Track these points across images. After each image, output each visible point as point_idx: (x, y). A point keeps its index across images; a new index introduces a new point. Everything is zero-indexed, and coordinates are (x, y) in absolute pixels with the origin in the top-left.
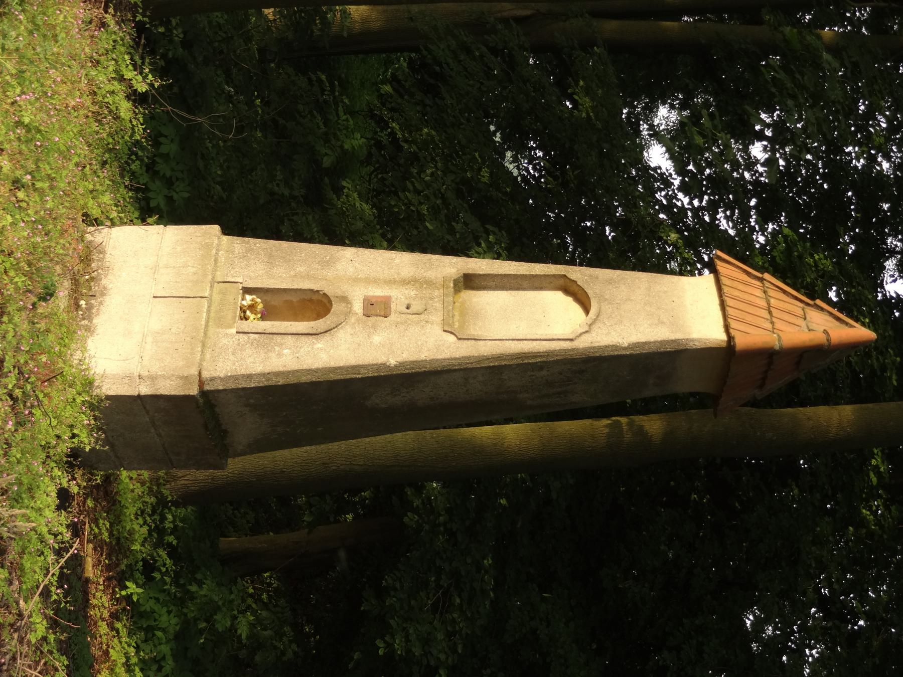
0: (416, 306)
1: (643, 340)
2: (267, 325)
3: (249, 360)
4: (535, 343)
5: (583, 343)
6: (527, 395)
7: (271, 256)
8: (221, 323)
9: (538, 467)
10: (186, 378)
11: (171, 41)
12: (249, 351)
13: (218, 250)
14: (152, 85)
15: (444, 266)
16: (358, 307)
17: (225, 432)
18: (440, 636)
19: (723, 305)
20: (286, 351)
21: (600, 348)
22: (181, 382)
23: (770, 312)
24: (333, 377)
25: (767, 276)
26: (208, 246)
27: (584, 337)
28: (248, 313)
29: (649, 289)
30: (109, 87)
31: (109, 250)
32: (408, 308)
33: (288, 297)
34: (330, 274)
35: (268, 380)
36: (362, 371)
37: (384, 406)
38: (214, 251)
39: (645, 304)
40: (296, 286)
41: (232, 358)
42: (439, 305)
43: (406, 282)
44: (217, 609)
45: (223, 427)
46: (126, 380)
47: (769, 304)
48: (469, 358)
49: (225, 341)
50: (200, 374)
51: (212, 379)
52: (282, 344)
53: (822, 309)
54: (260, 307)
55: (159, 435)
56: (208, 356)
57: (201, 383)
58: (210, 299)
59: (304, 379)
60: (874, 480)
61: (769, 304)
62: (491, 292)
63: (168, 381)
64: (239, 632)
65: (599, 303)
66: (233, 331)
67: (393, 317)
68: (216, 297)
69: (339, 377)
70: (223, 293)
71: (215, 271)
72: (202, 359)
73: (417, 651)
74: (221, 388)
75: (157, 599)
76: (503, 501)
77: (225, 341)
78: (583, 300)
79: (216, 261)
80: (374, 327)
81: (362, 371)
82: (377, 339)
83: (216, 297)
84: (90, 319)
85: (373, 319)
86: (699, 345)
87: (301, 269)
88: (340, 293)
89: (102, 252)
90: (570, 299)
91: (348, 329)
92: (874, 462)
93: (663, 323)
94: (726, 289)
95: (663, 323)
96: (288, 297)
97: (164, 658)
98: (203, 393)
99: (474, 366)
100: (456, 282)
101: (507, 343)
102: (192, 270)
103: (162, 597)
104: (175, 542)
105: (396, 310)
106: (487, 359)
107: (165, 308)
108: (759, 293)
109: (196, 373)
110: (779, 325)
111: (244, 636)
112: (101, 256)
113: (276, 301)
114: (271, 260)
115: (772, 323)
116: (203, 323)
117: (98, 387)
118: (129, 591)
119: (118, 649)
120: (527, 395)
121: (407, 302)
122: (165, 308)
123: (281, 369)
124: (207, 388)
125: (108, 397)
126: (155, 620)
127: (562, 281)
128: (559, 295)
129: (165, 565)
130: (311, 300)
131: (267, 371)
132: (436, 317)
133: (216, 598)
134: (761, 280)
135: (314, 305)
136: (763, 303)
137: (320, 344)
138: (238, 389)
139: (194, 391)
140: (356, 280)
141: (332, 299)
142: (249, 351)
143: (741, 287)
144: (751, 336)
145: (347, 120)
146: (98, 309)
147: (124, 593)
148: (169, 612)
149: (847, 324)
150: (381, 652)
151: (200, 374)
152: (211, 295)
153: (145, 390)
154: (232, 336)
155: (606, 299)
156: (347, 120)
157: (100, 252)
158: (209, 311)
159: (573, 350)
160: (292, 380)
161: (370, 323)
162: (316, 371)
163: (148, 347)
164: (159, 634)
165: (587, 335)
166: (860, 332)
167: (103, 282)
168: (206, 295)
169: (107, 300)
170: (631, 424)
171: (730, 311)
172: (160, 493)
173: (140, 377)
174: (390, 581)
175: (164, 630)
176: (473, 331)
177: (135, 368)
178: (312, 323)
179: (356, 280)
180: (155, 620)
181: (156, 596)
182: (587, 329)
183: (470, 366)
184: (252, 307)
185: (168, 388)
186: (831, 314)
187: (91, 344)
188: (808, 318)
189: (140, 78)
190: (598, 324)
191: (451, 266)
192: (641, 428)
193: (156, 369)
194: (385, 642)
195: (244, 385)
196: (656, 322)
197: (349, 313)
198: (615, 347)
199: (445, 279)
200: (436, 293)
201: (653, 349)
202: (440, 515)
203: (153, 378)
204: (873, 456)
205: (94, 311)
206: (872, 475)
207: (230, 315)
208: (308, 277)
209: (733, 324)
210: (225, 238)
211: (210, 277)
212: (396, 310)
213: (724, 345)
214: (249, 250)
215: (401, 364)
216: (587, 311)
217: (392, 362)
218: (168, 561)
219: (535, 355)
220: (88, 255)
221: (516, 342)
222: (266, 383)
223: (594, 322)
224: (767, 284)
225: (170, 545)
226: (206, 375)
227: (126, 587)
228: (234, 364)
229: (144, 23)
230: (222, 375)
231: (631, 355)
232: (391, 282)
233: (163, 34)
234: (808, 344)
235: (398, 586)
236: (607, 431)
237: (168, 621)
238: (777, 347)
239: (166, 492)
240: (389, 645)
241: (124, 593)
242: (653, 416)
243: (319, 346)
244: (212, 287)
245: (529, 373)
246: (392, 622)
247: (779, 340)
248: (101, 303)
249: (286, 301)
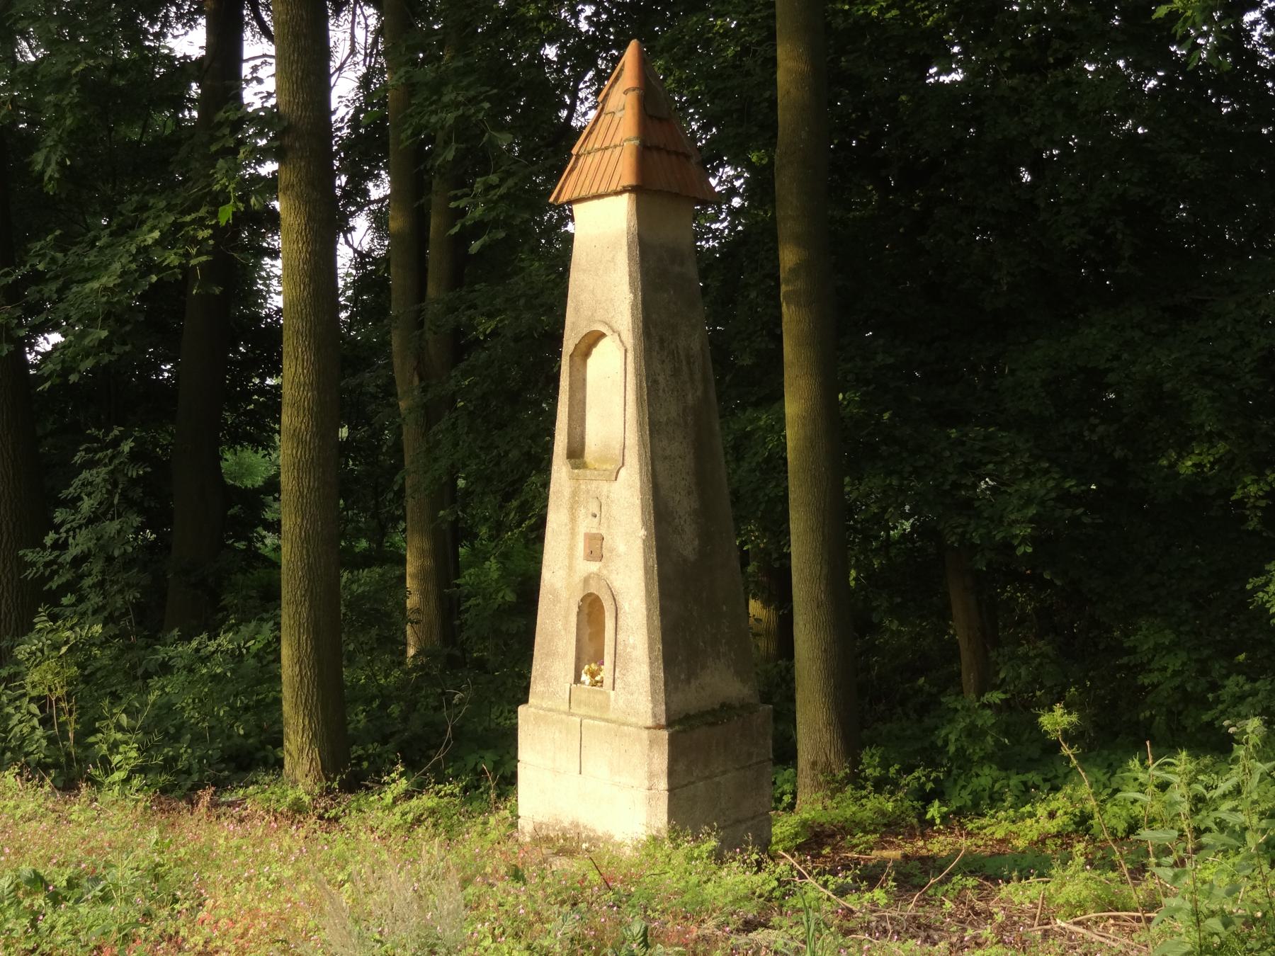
0: (594, 508)
1: (627, 278)
2: (608, 659)
5: (629, 339)
6: (690, 396)
8: (605, 707)
9: (829, 381)
10: (652, 742)
11: (379, 756)
12: (630, 678)
13: (542, 708)
14: (402, 775)
16: (594, 567)
17: (723, 705)
18: (1026, 486)
20: (631, 641)
21: (634, 322)
22: (656, 747)
23: (607, 148)
24: (656, 594)
25: (574, 151)
27: (624, 338)
28: (598, 678)
29: (584, 271)
30: (398, 816)
31: (538, 819)
33: (586, 638)
34: (564, 594)
35: (657, 659)
36: (650, 563)
37: (696, 542)
38: (541, 712)
40: (574, 630)
41: (636, 695)
42: (594, 484)
43: (573, 519)
44: (973, 724)
45: (717, 707)
46: (653, 803)
47: (598, 150)
48: (640, 455)
49: (621, 702)
50: (648, 728)
51: (654, 716)
53: (607, 95)
54: (594, 666)
55: (724, 773)
56: (634, 720)
57: (658, 727)
58: (583, 717)
59: (657, 623)
60: (894, 12)
61: (598, 150)
63: (655, 761)
64: (997, 701)
65: (595, 322)
66: (612, 693)
67: (603, 532)
68: (583, 711)
69: (656, 588)
70: (579, 704)
71: (559, 712)
72: (636, 726)
73: (1032, 511)
74: (663, 707)
75: (964, 787)
76: (886, 416)
77: (621, 702)
78: (594, 338)
79: (550, 710)
80: (611, 550)
82: (622, 548)
83: (583, 711)
84: (598, 838)
85: (605, 552)
86: (634, 222)
87: (559, 625)
88: (581, 585)
89: (541, 824)
90: (595, 351)
92: (875, 14)
94: (583, 194)
96: (586, 638)
97: (1024, 783)
98: (669, 724)
99: (648, 450)
100: (575, 467)
103: (961, 783)
104: (897, 767)
105: (599, 531)
106: (641, 436)
107: (591, 763)
108: (590, 159)
110: (617, 141)
111: (1003, 696)
113: (590, 649)
114: (550, 654)
115: (615, 146)
116: (603, 724)
117: (658, 831)
118: (937, 815)
119: (993, 829)
120: (690, 396)
122: (591, 763)
124: (663, 721)
125: (669, 822)
126: (984, 790)
127: (576, 359)
128: (590, 361)
129: (919, 778)
130: (589, 614)
132: (605, 487)
133: (962, 725)
134: (578, 156)
135: (592, 611)
137: (625, 606)
138: (666, 690)
139: (665, 734)
140: (571, 568)
143: (583, 177)
144: (623, 168)
145: (470, 575)
147: (938, 821)
148: (978, 775)
149: (621, 70)
150: (1029, 550)
151: (648, 728)
152: (579, 715)
153: (663, 784)
154: (617, 695)
156: (470, 575)
157: (541, 828)
158: (594, 718)
159: (635, 350)
160: (658, 635)
162: (649, 610)
164: (997, 786)
166: (630, 56)
167: (566, 824)
168: (578, 720)
169: (583, 820)
170: (788, 282)
171: (601, 190)
172: (842, 780)
173: (650, 789)
174: (953, 539)
175: (995, 782)
176: (617, 451)
177: (642, 794)
178: (607, 614)
179: (571, 568)
180: (984, 790)
181: (958, 788)
183: (649, 454)
184: (593, 675)
185: (661, 761)
186: (612, 86)
187: (618, 838)
189: (393, 785)
191: (560, 470)
192: (792, 270)
193: (642, 773)
194: (1019, 545)
195: (662, 684)
197: (598, 576)
198: (634, 307)
199: (571, 478)
200: (583, 487)
201: (636, 267)
202: (890, 484)
203: (651, 776)
204: (867, 15)
206: (888, 15)
207: (599, 697)
208: (566, 617)
209: (613, 187)
210: (531, 700)
211: (564, 716)
212: (599, 531)
213: (633, 196)
214: (542, 675)
215: (645, 524)
216: (603, 335)
217: (642, 533)
218: (916, 774)
219: (639, 388)
220: (541, 839)
222: (661, 661)
223: (611, 328)
224: (582, 151)
225: (898, 772)
226: (649, 723)
227: (933, 819)
229: (341, 780)
230: (650, 706)
231: (643, 290)
232: (573, 533)
233: (370, 763)
234: (636, 110)
235: (960, 530)
237: (986, 777)
238: (637, 142)
239: (841, 775)
240: (1024, 541)
241: (938, 821)
242: (781, 257)
244: (573, 715)
245: (661, 393)
246: (997, 538)
247: (629, 140)
248: (585, 827)
249: (590, 639)
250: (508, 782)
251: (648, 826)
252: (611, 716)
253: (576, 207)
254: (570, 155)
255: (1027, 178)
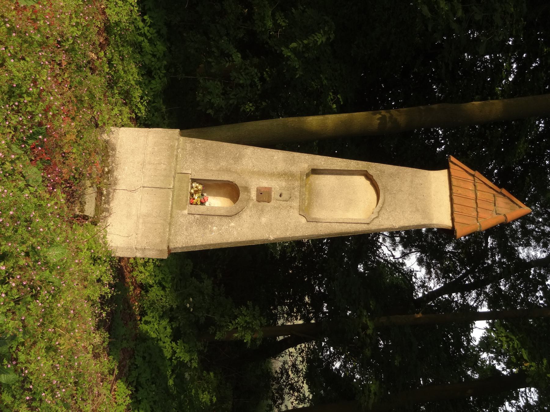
3: (195, 235)
4: (348, 225)
7: (206, 153)
10: (161, 251)
15: (301, 162)
16: (254, 194)
19: (451, 189)
24: (239, 245)
26: (172, 147)
29: (412, 182)
31: (118, 149)
32: (280, 196)
39: (409, 194)
41: (186, 233)
46: (129, 250)
48: (313, 235)
51: (175, 248)
52: (213, 223)
53: (504, 196)
59: (224, 246)
62: (326, 176)
66: (186, 212)
67: (273, 203)
81: (255, 242)
87: (223, 164)
90: (368, 183)
91: (248, 212)
93: (418, 210)
95: (418, 210)
101: (334, 225)
102: (164, 166)
107: (158, 193)
109: (166, 248)
112: (114, 152)
116: (170, 209)
121: (280, 192)
122: (158, 193)
123: (212, 242)
131: (204, 244)
132: (296, 204)
134: (473, 176)
136: (473, 196)
140: (253, 173)
141: (240, 189)
142: (194, 228)
146: (113, 195)
149: (520, 207)
151: (168, 247)
155: (388, 190)
161: (260, 208)
162: (231, 243)
163: (140, 227)
165: (377, 219)
182: (376, 215)
186: (509, 198)
188: (497, 205)
190: (383, 211)
193: (144, 245)
196: (415, 209)
197: (249, 199)
200: (297, 184)
205: (110, 196)
210: (182, 139)
217: (272, 238)
221: (338, 224)
224: (477, 180)
226: (172, 246)
228: (186, 238)
230: (180, 246)
232: (272, 175)
236: (379, 121)
243: (232, 224)
250: (140, 122)
251: (117, 247)
252: (174, 210)
253: (445, 172)
254: (474, 170)
255: (524, 56)
